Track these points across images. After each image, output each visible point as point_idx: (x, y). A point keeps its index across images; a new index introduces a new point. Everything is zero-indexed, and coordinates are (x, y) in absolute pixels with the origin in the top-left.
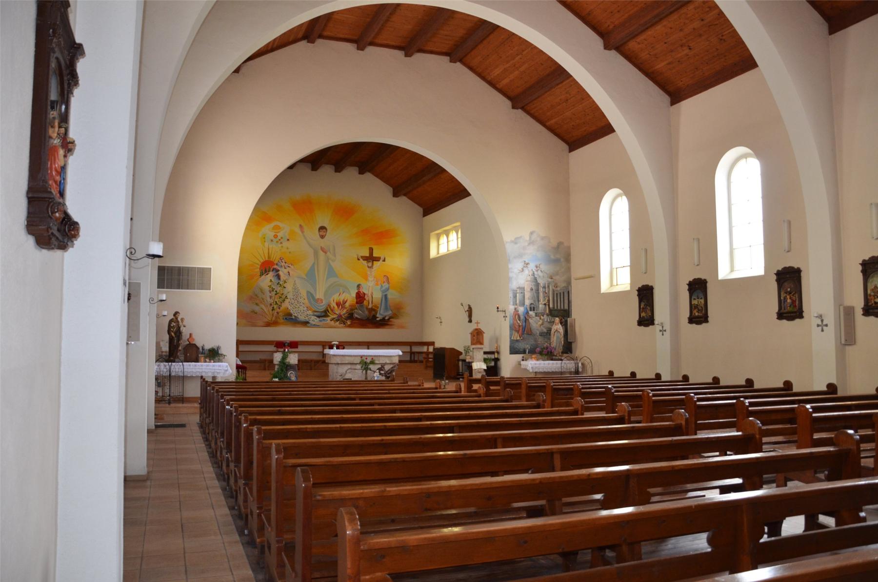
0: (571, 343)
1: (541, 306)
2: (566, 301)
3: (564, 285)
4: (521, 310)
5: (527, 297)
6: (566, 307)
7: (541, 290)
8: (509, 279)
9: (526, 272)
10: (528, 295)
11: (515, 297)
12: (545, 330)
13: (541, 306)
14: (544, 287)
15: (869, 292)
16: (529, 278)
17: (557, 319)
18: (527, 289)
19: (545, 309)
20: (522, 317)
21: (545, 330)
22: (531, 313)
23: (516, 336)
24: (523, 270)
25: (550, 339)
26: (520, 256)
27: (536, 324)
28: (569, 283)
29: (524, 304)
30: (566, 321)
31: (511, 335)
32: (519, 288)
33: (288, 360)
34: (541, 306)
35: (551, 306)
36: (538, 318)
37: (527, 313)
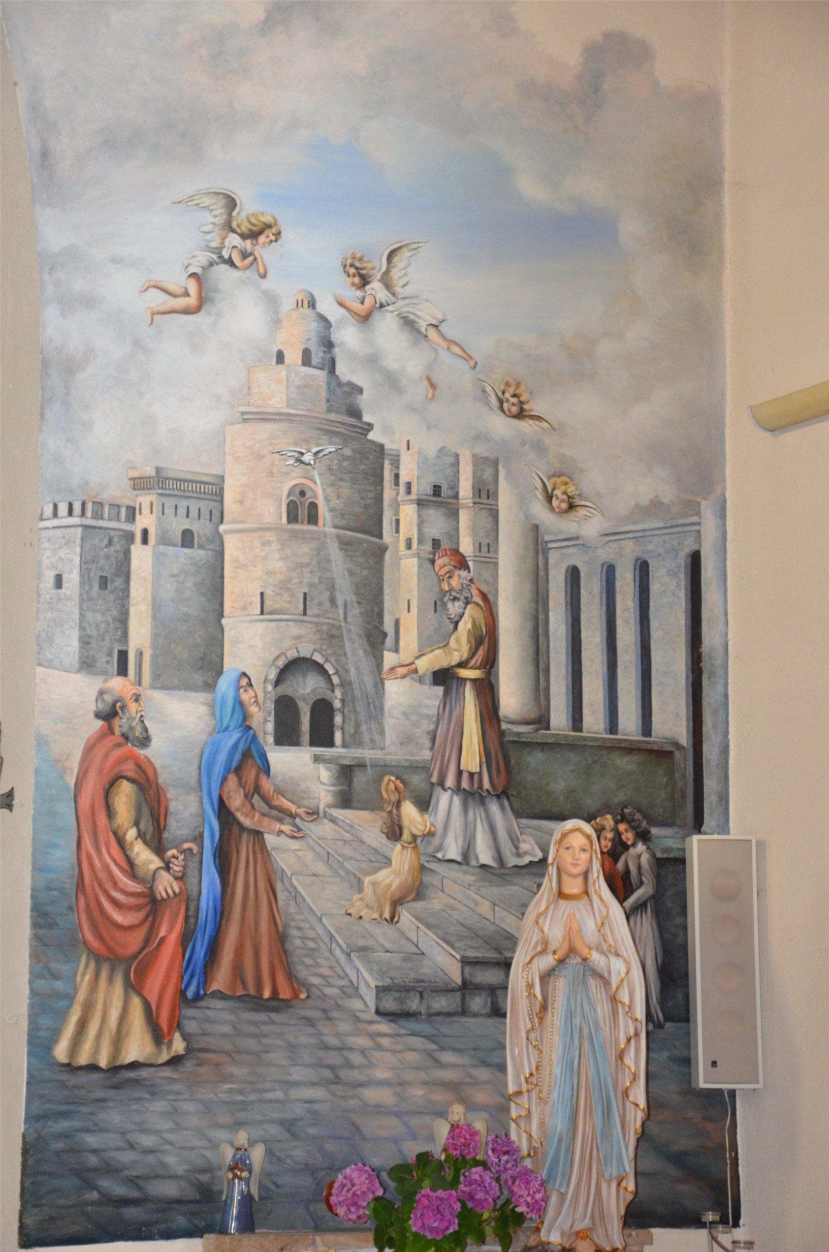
0: (720, 1104)
1: (404, 699)
2: (671, 661)
3: (646, 485)
4: (178, 725)
5: (241, 587)
6: (355, 804)
7: (405, 520)
8: (52, 378)
9: (243, 314)
10: (255, 564)
11: (109, 578)
12: (445, 963)
13: (396, 692)
14: (440, 498)
15: (722, 681)
16: (274, 390)
17: (576, 844)
18: (254, 500)
19: (445, 738)
20: (187, 810)
21: (445, 963)
22: (292, 764)
23: (114, 1025)
24: (201, 297)
25: (492, 1058)
26: (176, 134)
27: (332, 878)
28: (699, 471)
29: (207, 664)
30: (672, 867)
31: (46, 1009)
32: (158, 482)
33: (125, 782)
34: (404, 699)
35: (512, 699)
36: (367, 825)
37: (248, 761)
